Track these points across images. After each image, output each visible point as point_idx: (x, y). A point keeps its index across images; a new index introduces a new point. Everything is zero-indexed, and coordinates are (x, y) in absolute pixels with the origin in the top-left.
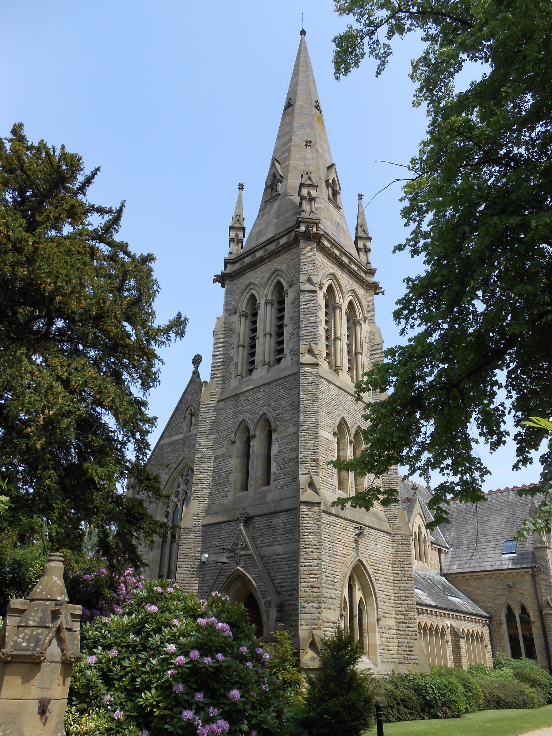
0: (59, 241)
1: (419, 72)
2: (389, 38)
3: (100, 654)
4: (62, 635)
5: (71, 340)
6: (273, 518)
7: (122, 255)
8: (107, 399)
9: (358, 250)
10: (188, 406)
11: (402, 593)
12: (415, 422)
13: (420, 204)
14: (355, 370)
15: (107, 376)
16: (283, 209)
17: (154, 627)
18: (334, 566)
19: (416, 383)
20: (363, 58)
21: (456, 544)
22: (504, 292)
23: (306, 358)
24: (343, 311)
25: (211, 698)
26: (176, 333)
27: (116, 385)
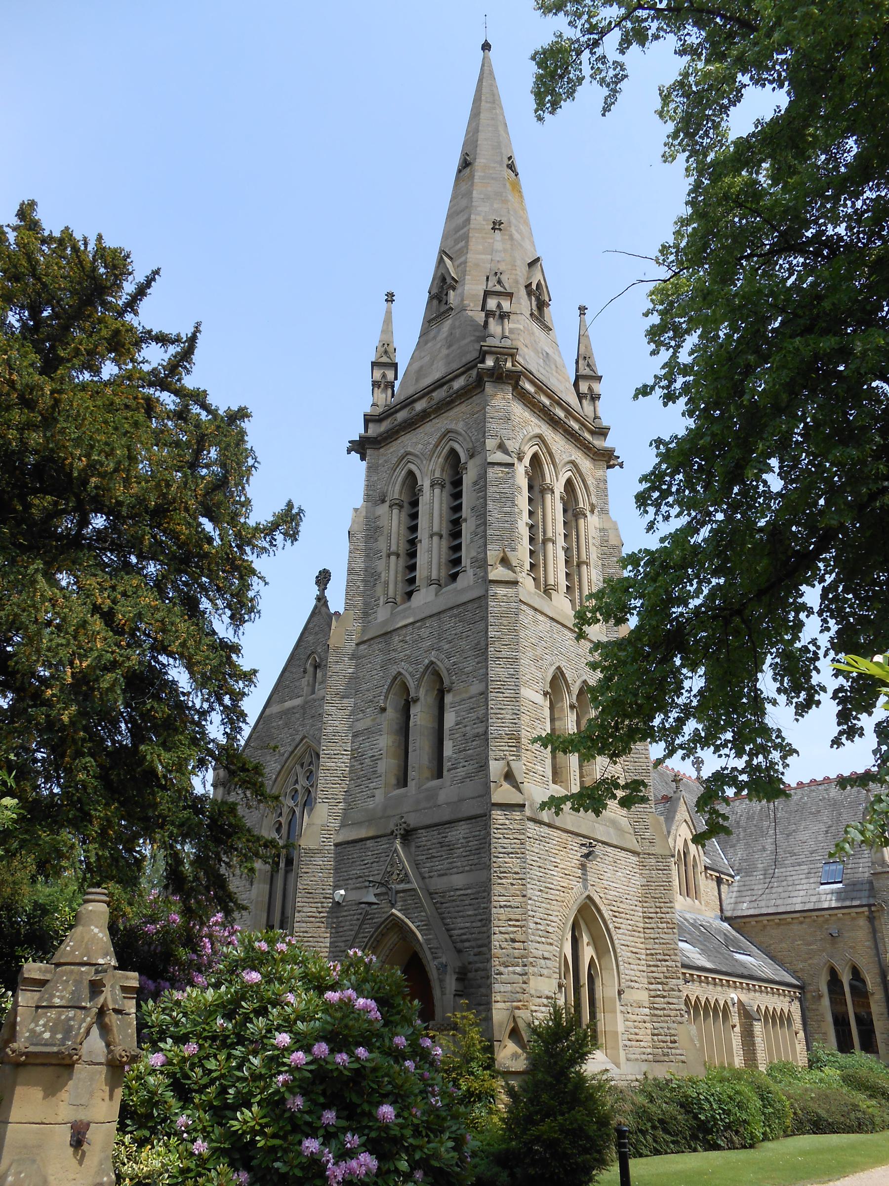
0: (95, 390)
1: (672, 106)
2: (622, 52)
3: (170, 1051)
4: (107, 1020)
5: (116, 547)
6: (447, 830)
7: (195, 409)
8: (174, 642)
9: (580, 397)
10: (310, 652)
11: (659, 949)
12: (672, 672)
13: (677, 320)
14: (577, 591)
15: (175, 604)
16: (458, 332)
17: (255, 1006)
18: (548, 906)
19: (674, 610)
20: (580, 84)
21: (746, 870)
22: (814, 459)
23: (498, 572)
24: (557, 495)
25: (348, 1118)
26: (285, 534)
27: (190, 619)
